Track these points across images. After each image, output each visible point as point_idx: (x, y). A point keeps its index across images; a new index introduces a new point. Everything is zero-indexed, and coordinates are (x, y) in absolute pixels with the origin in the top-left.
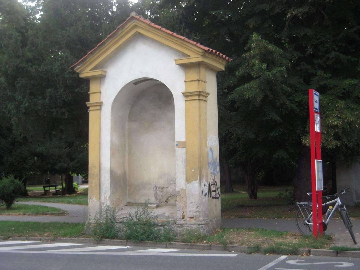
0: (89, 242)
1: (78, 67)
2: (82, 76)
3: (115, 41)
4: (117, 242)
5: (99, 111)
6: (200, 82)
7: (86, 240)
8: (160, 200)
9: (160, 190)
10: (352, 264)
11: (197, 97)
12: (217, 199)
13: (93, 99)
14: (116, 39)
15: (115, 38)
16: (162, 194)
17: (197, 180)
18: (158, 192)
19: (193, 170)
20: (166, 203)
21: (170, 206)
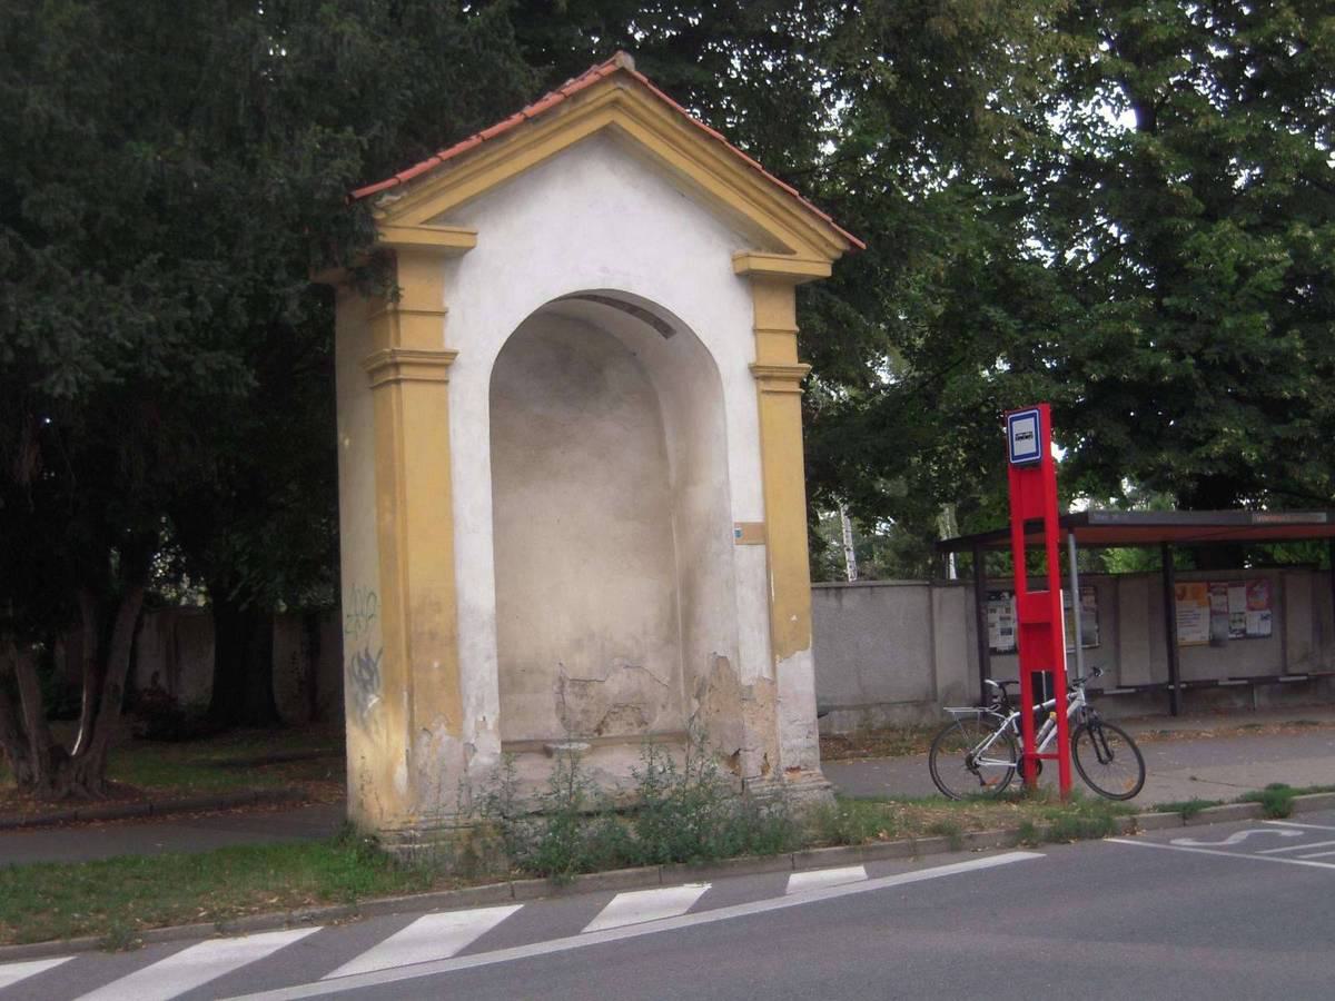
0: (513, 895)
3: (537, 135)
4: (626, 877)
7: (497, 889)
8: (578, 724)
9: (577, 689)
10: (1173, 842)
14: (546, 131)
15: (545, 126)
16: (583, 703)
17: (806, 648)
18: (570, 699)
19: (794, 618)
20: (596, 735)
21: (622, 743)
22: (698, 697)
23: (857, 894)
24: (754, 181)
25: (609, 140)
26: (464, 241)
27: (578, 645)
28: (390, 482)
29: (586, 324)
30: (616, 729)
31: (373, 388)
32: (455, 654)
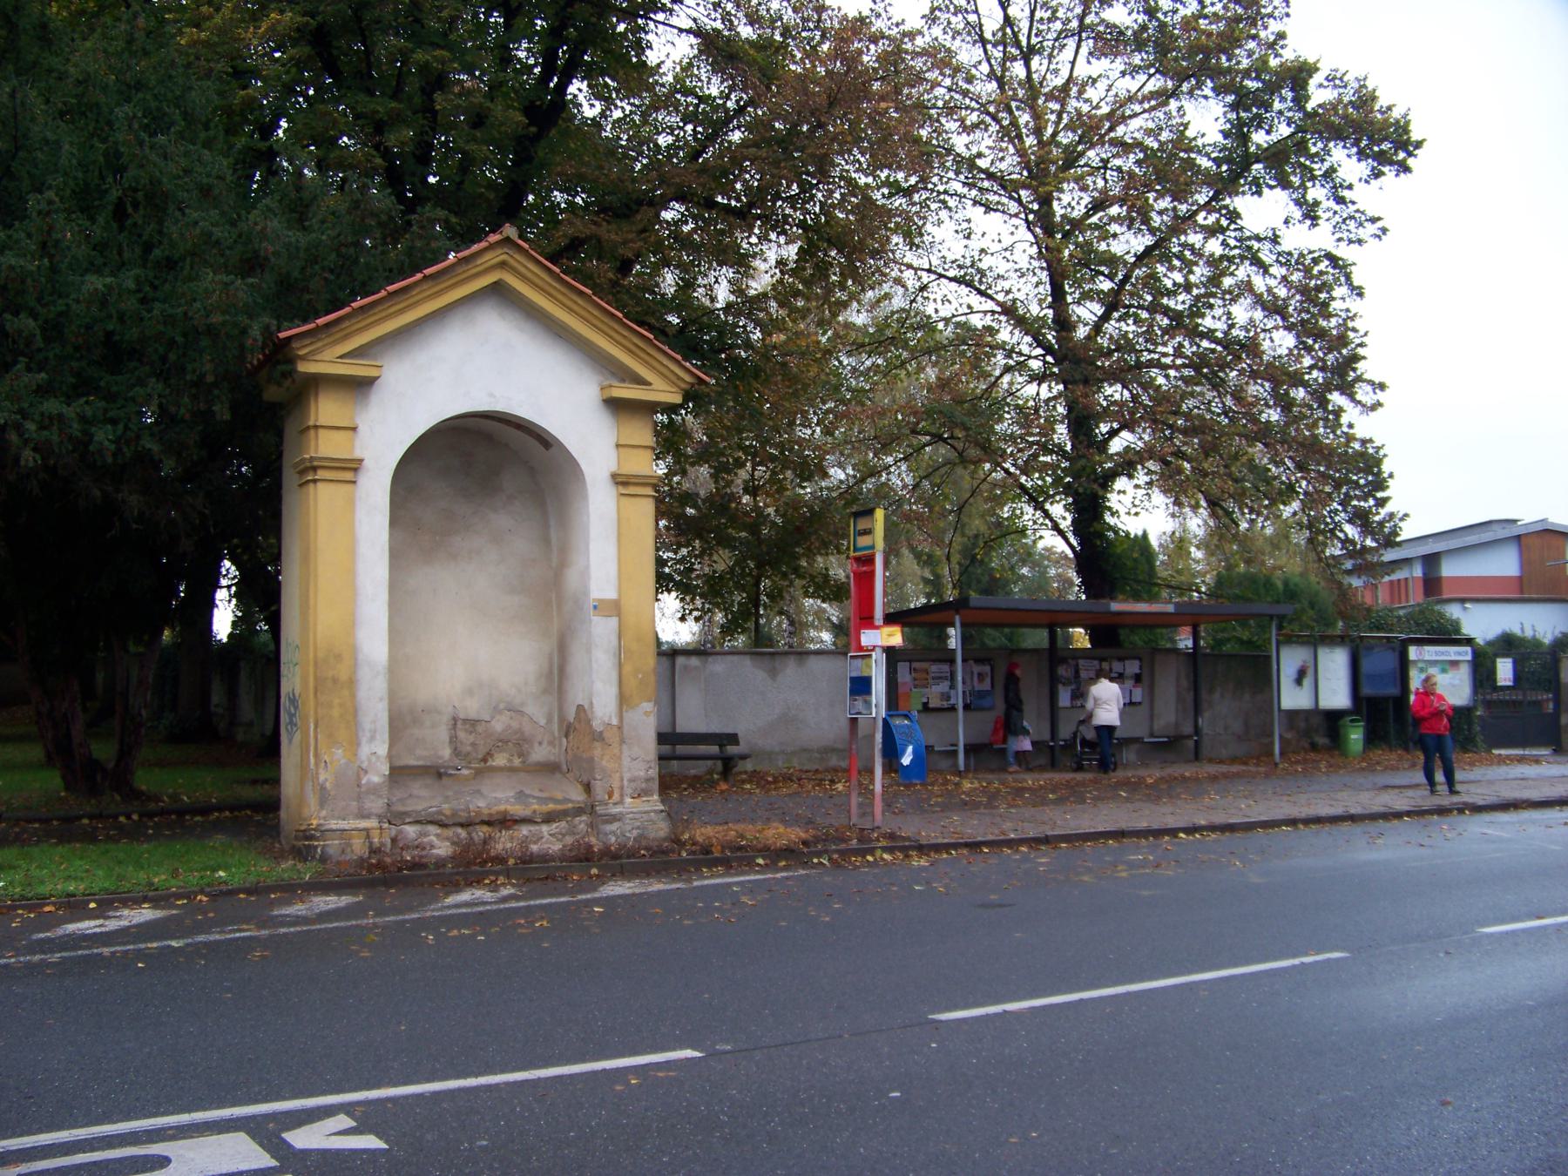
16: (471, 738)
18: (462, 735)
22: (567, 736)
23: (253, 1138)
24: (616, 326)
25: (498, 291)
26: (372, 373)
27: (469, 692)
28: (306, 558)
29: (489, 438)
30: (500, 760)
31: (301, 485)
32: (353, 696)
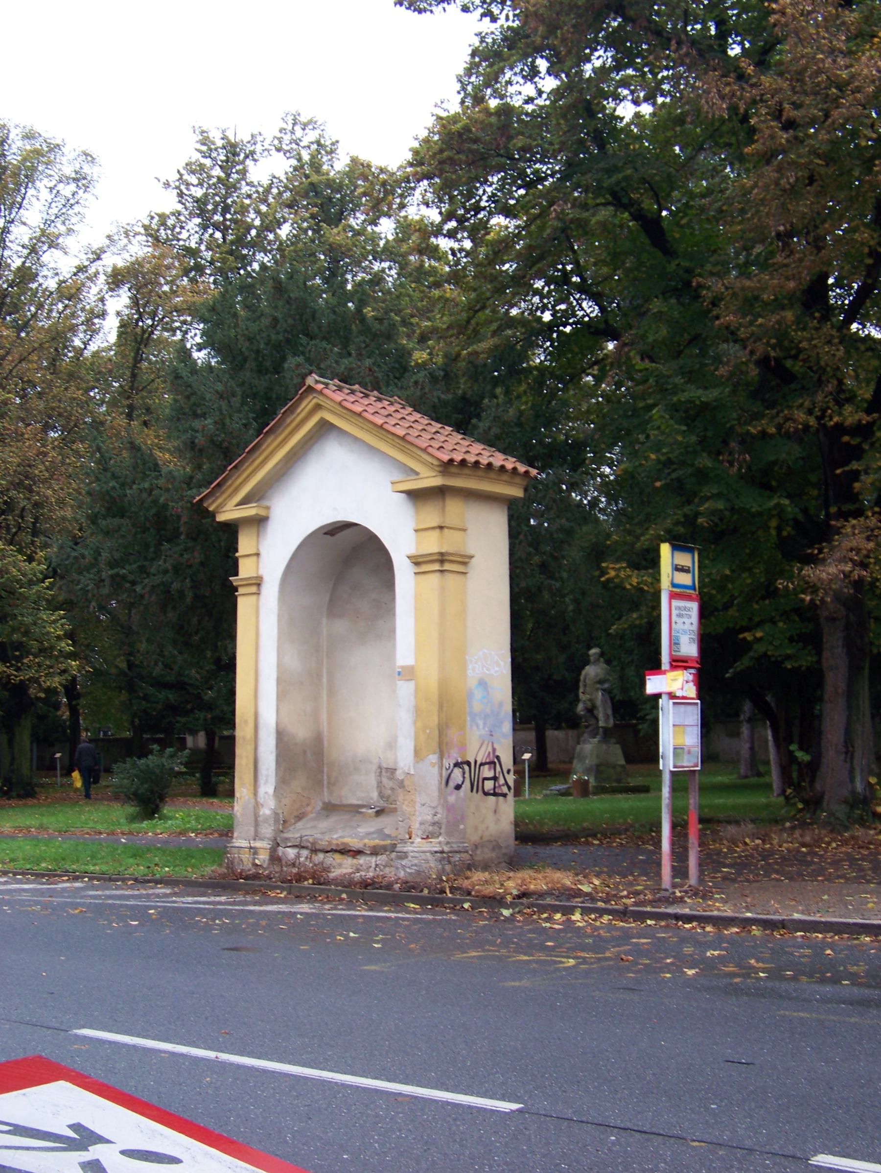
1: (210, 501)
2: (221, 518)
5: (254, 597)
6: (446, 530)
11: (437, 567)
12: (501, 798)
13: (246, 569)
18: (385, 780)
